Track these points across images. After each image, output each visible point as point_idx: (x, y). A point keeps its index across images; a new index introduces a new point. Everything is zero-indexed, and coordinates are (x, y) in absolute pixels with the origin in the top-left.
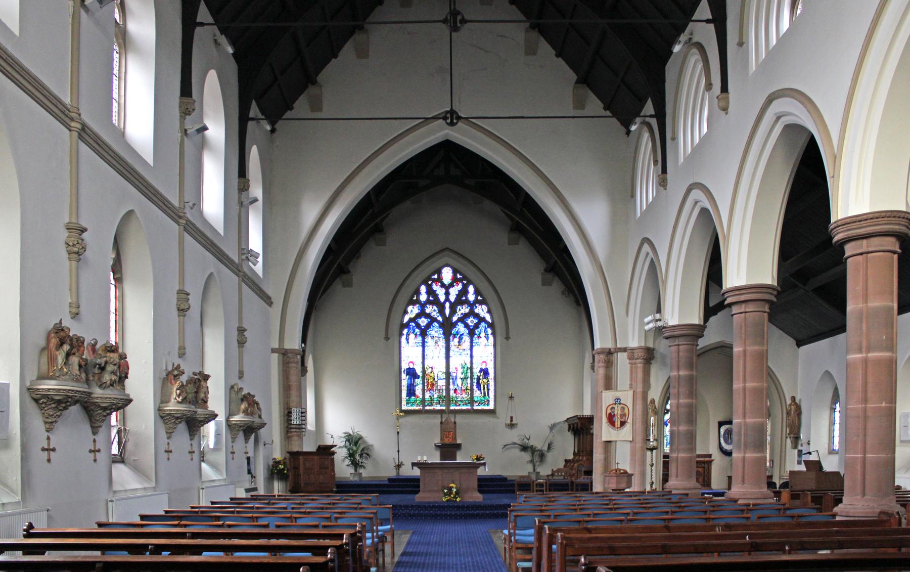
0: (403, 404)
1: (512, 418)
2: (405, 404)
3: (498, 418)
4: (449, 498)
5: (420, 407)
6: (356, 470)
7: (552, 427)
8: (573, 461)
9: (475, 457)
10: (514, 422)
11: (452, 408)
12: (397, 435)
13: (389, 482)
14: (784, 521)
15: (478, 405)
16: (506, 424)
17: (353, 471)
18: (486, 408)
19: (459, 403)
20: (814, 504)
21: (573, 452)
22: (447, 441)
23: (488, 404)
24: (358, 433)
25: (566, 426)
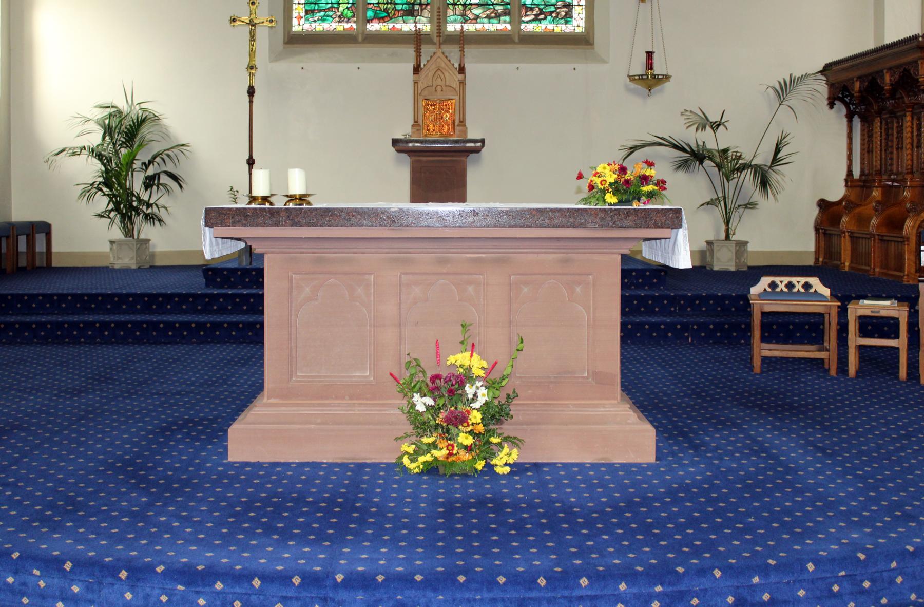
0: (295, 14)
1: (650, 55)
2: (303, 14)
3: (604, 61)
4: (441, 454)
5: (347, 26)
6: (129, 233)
7: (784, 90)
8: (846, 205)
9: (611, 178)
10: (658, 69)
11: (452, 27)
12: (247, 99)
13: (210, 282)
14: (137, 139)
15: (536, 19)
16: (632, 78)
17: (117, 233)
18: (560, 28)
19: (477, 11)
20: (683, 224)
21: (843, 174)
22: (434, 134)
23: (568, 17)
24: (143, 106)
25: (822, 88)
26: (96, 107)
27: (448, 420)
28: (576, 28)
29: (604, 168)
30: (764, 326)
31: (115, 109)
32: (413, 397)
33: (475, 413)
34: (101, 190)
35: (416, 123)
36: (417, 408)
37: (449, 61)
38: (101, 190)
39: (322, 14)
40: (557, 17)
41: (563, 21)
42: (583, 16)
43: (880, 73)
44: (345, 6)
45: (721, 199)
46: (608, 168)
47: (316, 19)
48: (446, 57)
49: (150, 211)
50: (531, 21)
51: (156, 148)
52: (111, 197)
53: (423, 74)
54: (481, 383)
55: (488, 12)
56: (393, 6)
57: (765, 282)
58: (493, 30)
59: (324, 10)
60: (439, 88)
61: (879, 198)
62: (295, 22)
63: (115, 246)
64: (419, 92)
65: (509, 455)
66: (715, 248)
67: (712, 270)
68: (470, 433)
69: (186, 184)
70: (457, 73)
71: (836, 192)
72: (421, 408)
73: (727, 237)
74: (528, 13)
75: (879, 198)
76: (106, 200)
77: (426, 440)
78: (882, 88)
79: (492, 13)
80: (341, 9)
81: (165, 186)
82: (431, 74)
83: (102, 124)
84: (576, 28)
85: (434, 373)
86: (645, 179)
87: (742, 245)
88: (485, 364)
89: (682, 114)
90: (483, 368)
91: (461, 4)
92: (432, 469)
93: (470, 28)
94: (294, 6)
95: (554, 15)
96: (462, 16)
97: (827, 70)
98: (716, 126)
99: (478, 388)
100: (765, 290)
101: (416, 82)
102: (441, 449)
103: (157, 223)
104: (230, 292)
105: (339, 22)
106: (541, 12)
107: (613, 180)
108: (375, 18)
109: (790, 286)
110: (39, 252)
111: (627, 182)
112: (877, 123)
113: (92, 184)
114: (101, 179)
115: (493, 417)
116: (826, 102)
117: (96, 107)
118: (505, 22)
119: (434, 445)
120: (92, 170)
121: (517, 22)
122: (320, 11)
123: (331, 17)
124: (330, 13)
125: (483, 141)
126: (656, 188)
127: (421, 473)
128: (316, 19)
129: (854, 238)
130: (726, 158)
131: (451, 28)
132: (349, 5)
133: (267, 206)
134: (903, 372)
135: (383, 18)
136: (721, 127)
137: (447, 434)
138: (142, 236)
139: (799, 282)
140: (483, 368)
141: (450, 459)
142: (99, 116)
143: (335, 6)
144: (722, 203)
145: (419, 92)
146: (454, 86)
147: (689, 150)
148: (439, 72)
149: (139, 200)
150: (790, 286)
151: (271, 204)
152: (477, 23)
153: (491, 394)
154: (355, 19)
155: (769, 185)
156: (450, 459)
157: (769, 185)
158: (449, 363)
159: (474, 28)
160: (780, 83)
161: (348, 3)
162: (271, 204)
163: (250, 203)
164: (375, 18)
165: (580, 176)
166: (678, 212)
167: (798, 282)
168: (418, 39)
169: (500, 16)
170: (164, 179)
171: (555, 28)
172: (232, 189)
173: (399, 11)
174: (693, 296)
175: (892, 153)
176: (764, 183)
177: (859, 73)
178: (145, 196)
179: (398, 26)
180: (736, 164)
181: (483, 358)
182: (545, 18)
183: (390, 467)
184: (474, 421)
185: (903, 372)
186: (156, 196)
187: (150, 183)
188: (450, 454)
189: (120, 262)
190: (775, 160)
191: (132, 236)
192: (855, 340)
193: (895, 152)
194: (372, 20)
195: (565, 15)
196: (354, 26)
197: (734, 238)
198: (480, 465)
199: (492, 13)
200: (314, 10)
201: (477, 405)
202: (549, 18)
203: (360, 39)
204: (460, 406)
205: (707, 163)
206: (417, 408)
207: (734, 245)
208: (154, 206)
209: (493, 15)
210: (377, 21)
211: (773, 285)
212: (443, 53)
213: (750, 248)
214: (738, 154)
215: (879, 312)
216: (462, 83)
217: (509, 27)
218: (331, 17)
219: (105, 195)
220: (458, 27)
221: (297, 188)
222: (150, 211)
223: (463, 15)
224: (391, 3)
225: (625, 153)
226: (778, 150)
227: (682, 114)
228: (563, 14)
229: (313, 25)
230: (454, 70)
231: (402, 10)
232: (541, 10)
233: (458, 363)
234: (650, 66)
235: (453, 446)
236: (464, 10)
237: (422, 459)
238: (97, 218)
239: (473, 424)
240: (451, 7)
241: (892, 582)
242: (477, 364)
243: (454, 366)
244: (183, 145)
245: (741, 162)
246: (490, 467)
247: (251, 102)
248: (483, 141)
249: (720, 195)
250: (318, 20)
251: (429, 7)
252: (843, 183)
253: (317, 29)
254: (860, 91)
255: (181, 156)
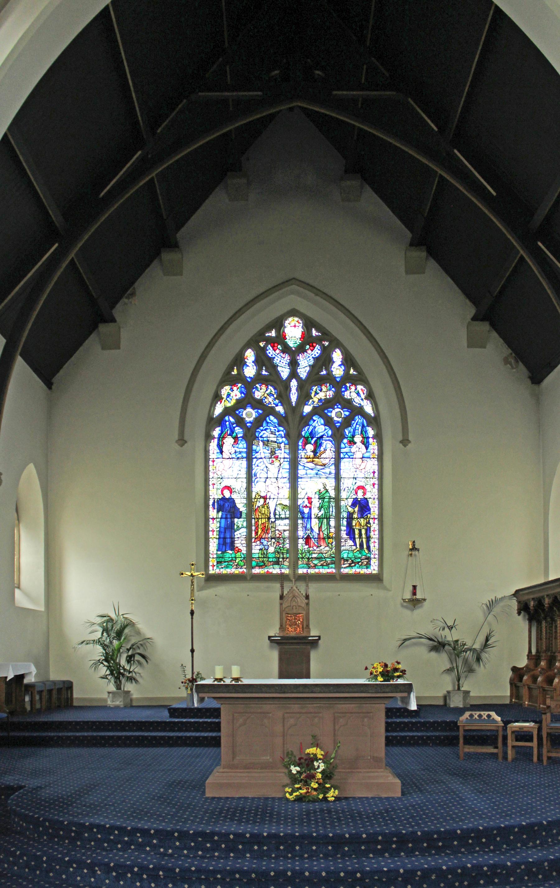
0: (211, 564)
1: (415, 587)
2: (215, 564)
4: (303, 791)
5: (241, 570)
6: (118, 687)
7: (491, 605)
9: (380, 669)
10: (419, 596)
12: (190, 617)
15: (350, 566)
17: (112, 687)
18: (364, 571)
19: (316, 562)
22: (292, 632)
23: (368, 565)
24: (125, 616)
25: (514, 604)
26: (98, 616)
27: (306, 777)
28: (373, 571)
29: (377, 665)
30: (465, 737)
31: (109, 618)
32: (290, 767)
33: (318, 774)
34: (102, 663)
35: (281, 626)
36: (292, 772)
37: (300, 592)
38: (102, 663)
39: (226, 563)
40: (362, 565)
41: (365, 567)
42: (377, 564)
43: (543, 597)
44: (240, 559)
45: (455, 667)
46: (379, 665)
47: (223, 566)
48: (298, 590)
49: (131, 675)
50: (347, 567)
51: (133, 640)
52: (108, 667)
53: (285, 600)
54: (321, 761)
55: (322, 562)
56: (267, 559)
57: (467, 714)
58: (325, 572)
59: (227, 562)
60: (294, 607)
61: (545, 667)
62: (211, 568)
63: (111, 695)
64: (283, 609)
65: (334, 792)
66: (451, 695)
67: (450, 707)
68: (317, 782)
69: (150, 660)
70: (304, 599)
71: (523, 663)
72: (294, 772)
73: (459, 689)
74: (345, 563)
75: (545, 667)
76: (105, 668)
77: (297, 786)
78: (544, 605)
79: (325, 563)
80: (237, 561)
81: (138, 661)
82: (290, 599)
83: (102, 626)
84: (373, 571)
85: (300, 757)
86: (396, 670)
87: (467, 693)
88: (323, 753)
89: (431, 622)
90: (322, 755)
91: (306, 558)
92: (300, 799)
93: (312, 571)
94: (210, 559)
95: (360, 564)
96: (307, 564)
97: (517, 593)
98: (450, 628)
99: (320, 763)
100: (467, 718)
101: (281, 604)
102: (303, 790)
103: (133, 681)
104: (176, 721)
105: (236, 568)
106: (353, 562)
107: (381, 670)
108: (257, 566)
109: (480, 716)
110: (76, 698)
111: (388, 671)
112: (544, 624)
113: (99, 660)
114: (104, 658)
115: (327, 776)
116: (516, 612)
117: (98, 616)
118: (332, 568)
119: (300, 788)
120: (98, 652)
121: (339, 567)
122: (225, 562)
123: (231, 565)
124: (231, 563)
125: (319, 637)
126: (401, 674)
127: (295, 800)
128: (223, 566)
129: (530, 689)
130: (458, 645)
131: (301, 571)
132: (242, 559)
133: (222, 683)
134: (535, 759)
135: (261, 566)
136: (454, 628)
137: (306, 783)
138: (126, 689)
139: (485, 714)
140: (322, 755)
141: (308, 794)
142: (99, 622)
143: (234, 559)
144: (456, 670)
145: (283, 609)
146: (303, 606)
147: (436, 640)
148: (294, 598)
149: (125, 670)
150: (480, 716)
151: (224, 682)
152: (316, 568)
153: (326, 766)
154: (245, 567)
155: (482, 660)
156: (308, 794)
157: (482, 660)
158: (306, 752)
159: (314, 571)
160: (489, 601)
161: (241, 558)
162: (224, 682)
163: (214, 681)
164: (257, 566)
165: (366, 668)
166: (410, 685)
167: (484, 714)
168: (282, 578)
169: (329, 564)
170: (137, 657)
171: (361, 571)
172: (182, 665)
173: (270, 562)
174: (441, 722)
175: (552, 640)
176: (478, 659)
177: (532, 596)
178: (127, 667)
179: (270, 571)
180: (463, 648)
181: (322, 750)
182: (355, 566)
183: (280, 799)
184: (318, 777)
185: (535, 759)
186: (135, 668)
187: (130, 659)
188: (308, 792)
189: (114, 703)
190: (486, 644)
191: (120, 689)
192: (510, 742)
193: (554, 641)
194: (255, 567)
195: (366, 564)
196: (245, 570)
197: (462, 689)
198: (321, 796)
199: (325, 563)
200: (222, 561)
201: (319, 770)
202: (357, 565)
203: (248, 578)
204: (312, 771)
205: (447, 647)
206: (292, 772)
207: (462, 693)
208: (133, 673)
209: (325, 564)
210: (258, 567)
211: (471, 716)
212: (297, 588)
213: (472, 694)
214: (464, 643)
215: (523, 729)
216: (308, 604)
217: (334, 571)
218: (231, 565)
219: (105, 666)
220: (305, 571)
221: (235, 675)
222: (131, 675)
223: (307, 564)
224: (266, 558)
225: (400, 642)
226: (487, 640)
227: (431, 622)
228: (365, 563)
229: (221, 570)
230: (303, 597)
231: (272, 561)
232: (352, 561)
233: (311, 753)
234: (414, 594)
235: (308, 788)
236: (308, 561)
237: (295, 794)
238: (100, 679)
239: (318, 779)
240: (300, 559)
241: (495, 839)
242: (319, 753)
243: (308, 754)
244: (148, 639)
245: (466, 647)
246: (325, 799)
247: (192, 618)
248: (319, 637)
249: (455, 665)
250: (224, 567)
251: (288, 560)
252: (526, 657)
253: (224, 573)
254: (534, 606)
255: (148, 645)
